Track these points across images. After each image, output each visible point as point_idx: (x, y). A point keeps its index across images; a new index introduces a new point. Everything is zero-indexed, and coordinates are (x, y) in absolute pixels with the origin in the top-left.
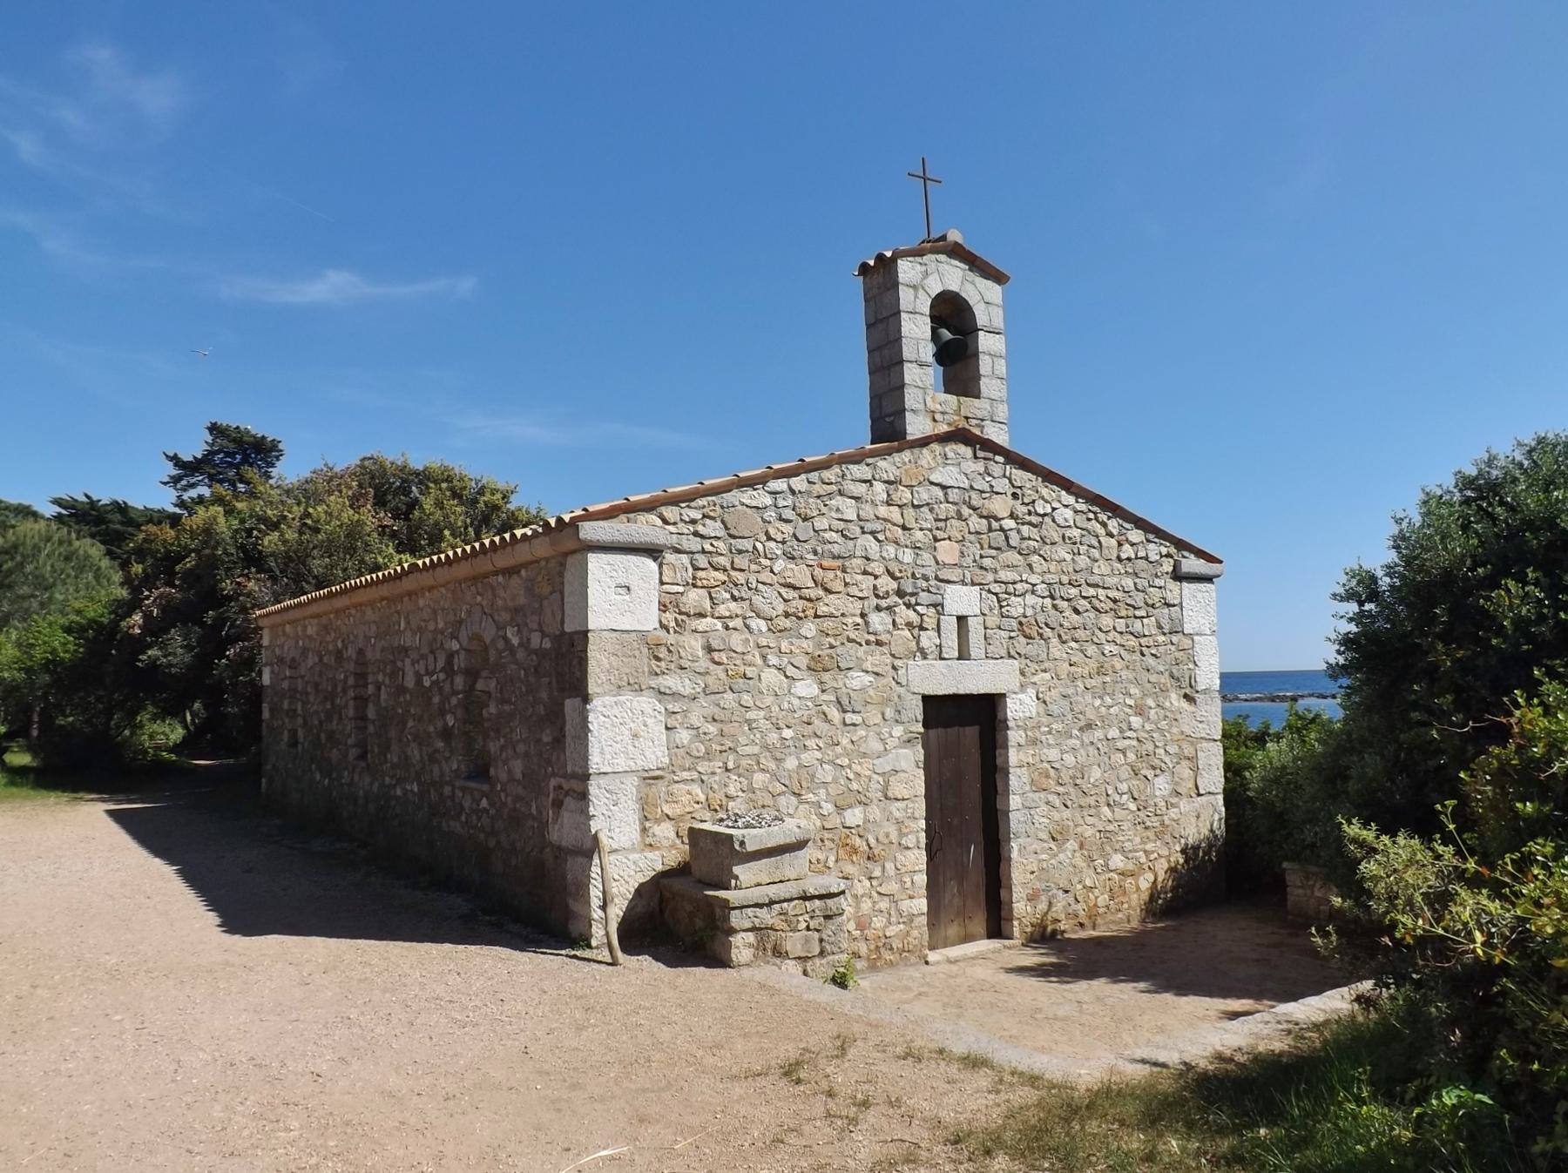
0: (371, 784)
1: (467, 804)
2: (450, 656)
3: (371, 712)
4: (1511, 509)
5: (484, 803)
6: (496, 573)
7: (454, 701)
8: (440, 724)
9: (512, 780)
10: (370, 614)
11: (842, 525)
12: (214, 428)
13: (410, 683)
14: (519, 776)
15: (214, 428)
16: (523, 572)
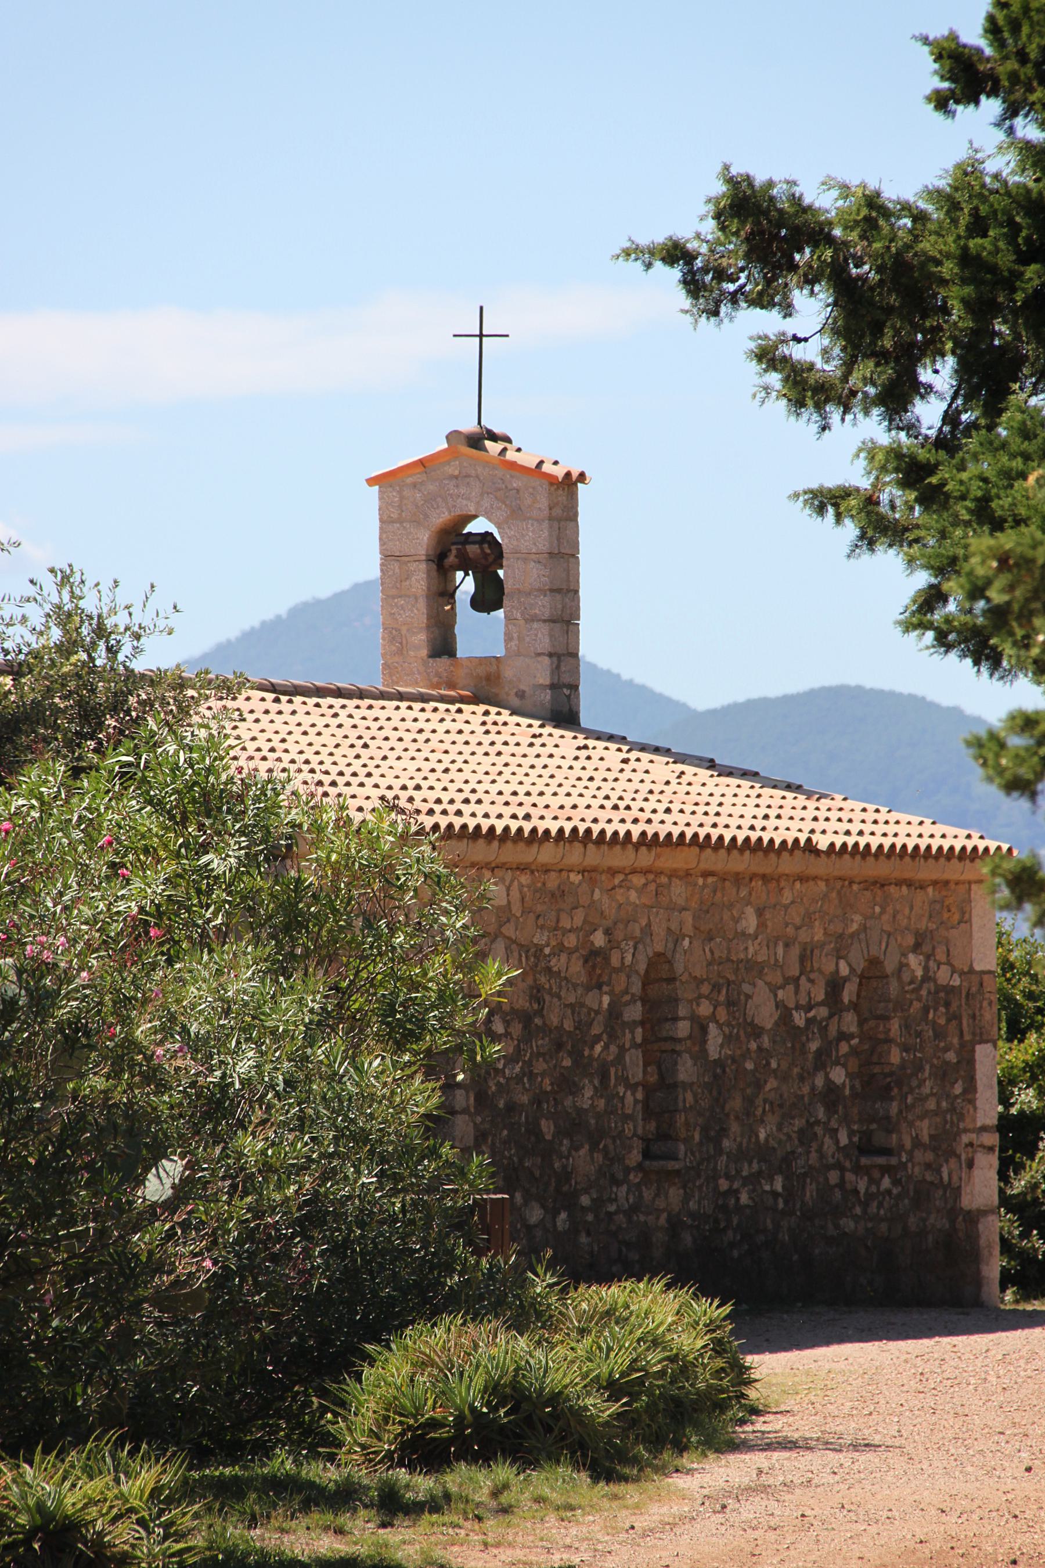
0: (686, 1200)
1: (862, 1186)
2: (835, 986)
3: (686, 1070)
4: (277, 981)
5: (886, 1183)
6: (899, 883)
7: (844, 1048)
8: (819, 1081)
9: (917, 1143)
10: (678, 891)
11: (771, 945)
12: (371, 481)
13: (765, 1015)
14: (926, 1139)
15: (371, 481)
16: (930, 890)
